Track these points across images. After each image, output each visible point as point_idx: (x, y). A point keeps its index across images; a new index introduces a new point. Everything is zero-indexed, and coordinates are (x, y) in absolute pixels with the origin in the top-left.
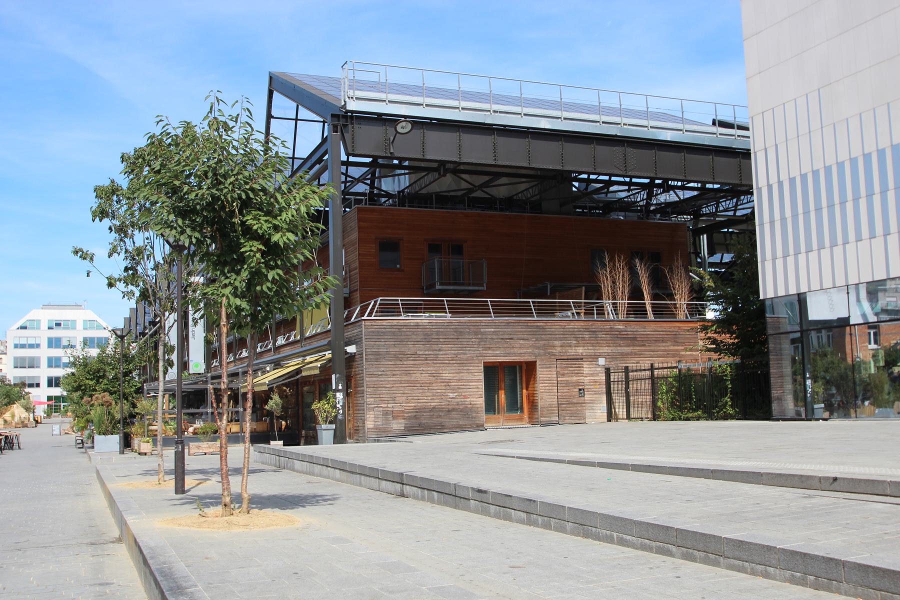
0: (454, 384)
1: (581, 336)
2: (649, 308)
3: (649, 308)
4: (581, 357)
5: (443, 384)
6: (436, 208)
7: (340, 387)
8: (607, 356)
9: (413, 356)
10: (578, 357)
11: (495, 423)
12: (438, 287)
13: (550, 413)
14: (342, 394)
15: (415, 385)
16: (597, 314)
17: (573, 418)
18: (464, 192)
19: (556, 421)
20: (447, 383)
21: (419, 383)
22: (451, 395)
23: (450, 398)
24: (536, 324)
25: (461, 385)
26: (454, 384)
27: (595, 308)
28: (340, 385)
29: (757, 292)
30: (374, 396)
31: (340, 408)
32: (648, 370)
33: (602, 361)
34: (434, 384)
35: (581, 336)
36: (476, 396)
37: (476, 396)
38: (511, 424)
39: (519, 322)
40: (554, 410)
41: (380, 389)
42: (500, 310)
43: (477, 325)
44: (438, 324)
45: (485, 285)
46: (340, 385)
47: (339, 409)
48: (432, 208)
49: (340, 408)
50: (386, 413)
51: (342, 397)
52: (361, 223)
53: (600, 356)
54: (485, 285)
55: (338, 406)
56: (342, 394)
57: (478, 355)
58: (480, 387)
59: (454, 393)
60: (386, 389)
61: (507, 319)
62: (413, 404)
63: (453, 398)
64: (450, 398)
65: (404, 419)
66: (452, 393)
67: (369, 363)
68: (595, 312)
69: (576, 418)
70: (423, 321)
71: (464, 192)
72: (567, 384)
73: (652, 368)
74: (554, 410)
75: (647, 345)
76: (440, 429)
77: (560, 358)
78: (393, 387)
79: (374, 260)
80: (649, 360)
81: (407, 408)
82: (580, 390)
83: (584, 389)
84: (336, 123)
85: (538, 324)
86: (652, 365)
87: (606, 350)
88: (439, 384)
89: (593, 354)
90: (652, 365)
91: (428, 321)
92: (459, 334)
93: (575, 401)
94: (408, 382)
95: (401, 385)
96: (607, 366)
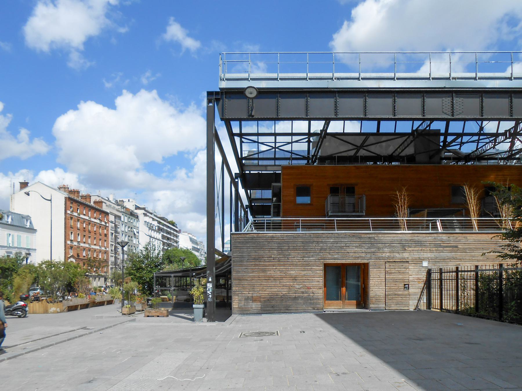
0: (300, 279)
1: (407, 245)
2: (475, 224)
3: (475, 224)
4: (407, 260)
5: (291, 279)
6: (337, 164)
7: (210, 280)
8: (428, 259)
9: (269, 259)
10: (404, 260)
11: (337, 306)
12: (330, 214)
13: (378, 302)
14: (211, 284)
15: (269, 279)
16: (432, 228)
17: (398, 305)
18: (375, 155)
19: (383, 307)
20: (295, 279)
21: (273, 277)
22: (297, 286)
23: (296, 289)
24: (368, 236)
25: (306, 280)
26: (300, 279)
27: (430, 224)
28: (210, 278)
29: (243, 121)
30: (238, 286)
31: (210, 293)
32: (455, 272)
33: (425, 264)
34: (284, 279)
35: (407, 245)
36: (317, 288)
37: (317, 288)
38: (350, 307)
39: (354, 236)
40: (382, 300)
41: (243, 281)
42: (342, 226)
43: (318, 236)
44: (288, 236)
45: (364, 212)
46: (210, 278)
47: (209, 295)
48: (335, 164)
49: (210, 293)
50: (247, 299)
51: (211, 286)
52: (284, 176)
53: (424, 259)
54: (364, 212)
55: (208, 292)
56: (211, 284)
57: (319, 258)
58: (320, 281)
59: (300, 285)
60: (248, 281)
61: (344, 232)
62: (267, 292)
63: (299, 289)
64: (296, 289)
65: (261, 302)
66: (298, 285)
67: (235, 263)
68: (430, 226)
69: (400, 306)
70: (277, 234)
71: (375, 155)
72: (395, 281)
73: (457, 271)
74: (382, 300)
75: (468, 251)
76: (287, 310)
77: (389, 260)
78: (253, 280)
79: (293, 199)
80: (469, 263)
81: (264, 295)
82: (405, 285)
83: (408, 285)
84: (210, 98)
85: (371, 236)
86: (457, 268)
87: (429, 255)
88: (289, 279)
89: (418, 258)
90: (457, 268)
91: (280, 234)
92: (306, 243)
93: (400, 293)
94: (265, 276)
95: (259, 279)
96: (430, 268)
